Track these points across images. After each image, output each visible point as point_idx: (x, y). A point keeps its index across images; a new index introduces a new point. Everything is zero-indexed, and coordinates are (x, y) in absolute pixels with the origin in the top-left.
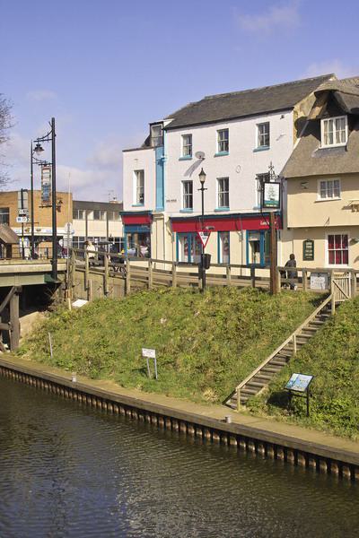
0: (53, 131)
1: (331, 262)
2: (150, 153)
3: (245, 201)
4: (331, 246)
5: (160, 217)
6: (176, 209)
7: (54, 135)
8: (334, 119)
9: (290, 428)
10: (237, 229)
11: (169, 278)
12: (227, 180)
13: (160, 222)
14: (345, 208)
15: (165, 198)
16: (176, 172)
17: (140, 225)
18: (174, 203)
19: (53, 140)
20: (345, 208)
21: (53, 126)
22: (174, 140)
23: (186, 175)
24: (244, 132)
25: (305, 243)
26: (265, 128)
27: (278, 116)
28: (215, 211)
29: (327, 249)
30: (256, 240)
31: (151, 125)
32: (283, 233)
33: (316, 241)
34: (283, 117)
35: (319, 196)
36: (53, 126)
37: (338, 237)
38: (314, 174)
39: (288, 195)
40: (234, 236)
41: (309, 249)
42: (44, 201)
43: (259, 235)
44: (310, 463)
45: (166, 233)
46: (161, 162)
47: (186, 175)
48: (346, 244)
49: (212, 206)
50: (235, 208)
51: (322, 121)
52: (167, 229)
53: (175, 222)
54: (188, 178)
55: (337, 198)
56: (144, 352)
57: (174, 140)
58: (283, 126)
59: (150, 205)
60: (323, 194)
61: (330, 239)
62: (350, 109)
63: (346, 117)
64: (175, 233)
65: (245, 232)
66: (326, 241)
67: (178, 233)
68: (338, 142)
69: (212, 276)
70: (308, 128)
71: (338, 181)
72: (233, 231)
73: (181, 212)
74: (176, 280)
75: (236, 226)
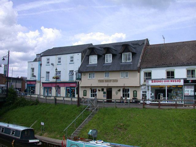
1: (91, 97)
2: (37, 63)
6: (44, 80)
7: (9, 56)
9: (48, 138)
12: (49, 73)
16: (45, 68)
21: (9, 53)
22: (44, 59)
24: (65, 58)
25: (84, 91)
27: (77, 54)
31: (37, 55)
36: (9, 53)
38: (88, 71)
41: (135, 93)
46: (41, 65)
49: (51, 80)
51: (123, 54)
56: (41, 123)
58: (78, 57)
68: (128, 60)
69: (58, 100)
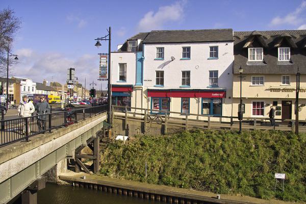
0: (110, 34)
1: (254, 114)
3: (201, 82)
4: (254, 107)
5: (140, 89)
6: (152, 85)
8: (256, 48)
10: (195, 97)
11: (206, 124)
13: (139, 92)
14: (266, 90)
15: (144, 79)
17: (123, 92)
18: (150, 82)
19: (110, 40)
20: (266, 90)
23: (158, 68)
24: (200, 50)
26: (161, 51)
28: (180, 87)
29: (252, 108)
30: (207, 102)
32: (227, 99)
33: (246, 104)
34: (227, 44)
35: (252, 83)
37: (258, 103)
39: (234, 82)
40: (193, 101)
42: (101, 76)
43: (210, 100)
44: (124, 192)
45: (143, 97)
47: (158, 68)
48: (263, 106)
50: (194, 85)
51: (249, 49)
52: (144, 95)
53: (150, 92)
54: (160, 70)
55: (262, 85)
57: (150, 50)
58: (227, 51)
59: (130, 80)
60: (253, 84)
61: (254, 104)
62: (267, 44)
63: (262, 49)
64: (150, 98)
65: (201, 99)
66: (252, 105)
67: (152, 98)
68: (257, 59)
70: (240, 51)
71: (263, 77)
72: (192, 97)
73: (154, 86)
74: (211, 125)
75: (195, 95)
